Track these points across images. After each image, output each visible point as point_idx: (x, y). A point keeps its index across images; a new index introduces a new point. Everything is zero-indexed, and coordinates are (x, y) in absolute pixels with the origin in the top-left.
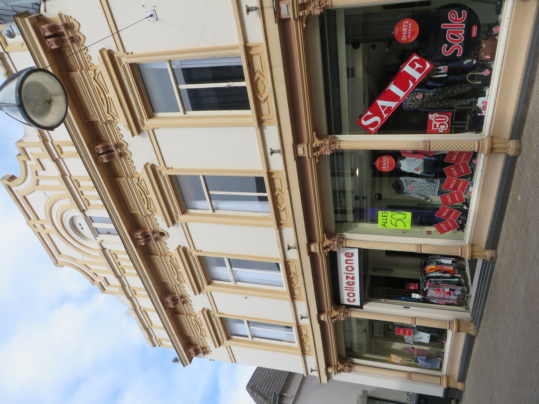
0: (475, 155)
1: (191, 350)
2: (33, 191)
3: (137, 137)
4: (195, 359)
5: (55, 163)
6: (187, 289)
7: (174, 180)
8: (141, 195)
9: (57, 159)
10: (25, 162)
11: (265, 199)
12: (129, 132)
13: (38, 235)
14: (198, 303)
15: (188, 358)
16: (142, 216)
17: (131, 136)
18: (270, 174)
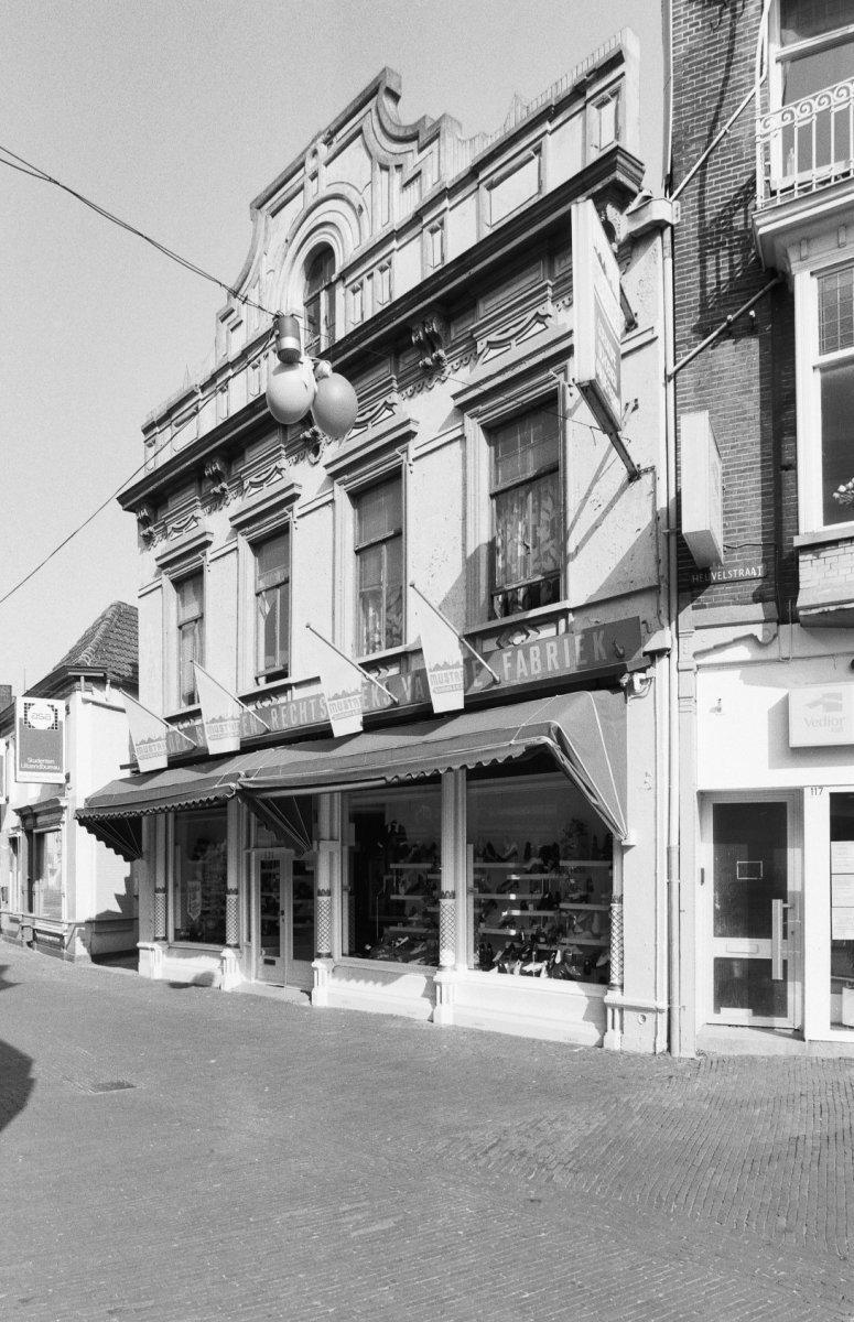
0: (593, 967)
1: (144, 513)
2: (371, 156)
3: (155, 565)
4: (132, 518)
5: (239, 354)
6: (236, 505)
7: (395, 477)
8: (370, 410)
9: (584, 94)
10: (415, 137)
11: (492, 616)
12: (460, 388)
13: (298, 164)
14: (216, 524)
15: (134, 504)
16: (166, 519)
17: (453, 393)
18: (288, 687)
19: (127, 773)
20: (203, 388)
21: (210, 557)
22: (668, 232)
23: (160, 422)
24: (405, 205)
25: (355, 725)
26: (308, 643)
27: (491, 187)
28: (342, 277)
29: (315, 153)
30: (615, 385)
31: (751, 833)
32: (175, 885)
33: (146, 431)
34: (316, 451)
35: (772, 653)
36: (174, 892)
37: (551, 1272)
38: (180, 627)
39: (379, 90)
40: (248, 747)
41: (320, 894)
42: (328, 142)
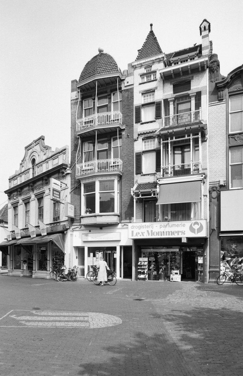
10: (45, 148)
14: (20, 199)
19: (6, 240)
20: (18, 175)
21: (19, 204)
22: (70, 174)
23: (11, 179)
24: (44, 158)
25: (46, 234)
26: (30, 221)
27: (53, 160)
28: (37, 165)
29: (33, 144)
30: (211, 233)
31: (80, 250)
32: (14, 260)
33: (9, 180)
34: (33, 191)
35: (81, 229)
36: (14, 261)
37: (6, 356)
38: (15, 215)
39: (42, 138)
40: (22, 238)
41: (34, 260)
42: (35, 143)
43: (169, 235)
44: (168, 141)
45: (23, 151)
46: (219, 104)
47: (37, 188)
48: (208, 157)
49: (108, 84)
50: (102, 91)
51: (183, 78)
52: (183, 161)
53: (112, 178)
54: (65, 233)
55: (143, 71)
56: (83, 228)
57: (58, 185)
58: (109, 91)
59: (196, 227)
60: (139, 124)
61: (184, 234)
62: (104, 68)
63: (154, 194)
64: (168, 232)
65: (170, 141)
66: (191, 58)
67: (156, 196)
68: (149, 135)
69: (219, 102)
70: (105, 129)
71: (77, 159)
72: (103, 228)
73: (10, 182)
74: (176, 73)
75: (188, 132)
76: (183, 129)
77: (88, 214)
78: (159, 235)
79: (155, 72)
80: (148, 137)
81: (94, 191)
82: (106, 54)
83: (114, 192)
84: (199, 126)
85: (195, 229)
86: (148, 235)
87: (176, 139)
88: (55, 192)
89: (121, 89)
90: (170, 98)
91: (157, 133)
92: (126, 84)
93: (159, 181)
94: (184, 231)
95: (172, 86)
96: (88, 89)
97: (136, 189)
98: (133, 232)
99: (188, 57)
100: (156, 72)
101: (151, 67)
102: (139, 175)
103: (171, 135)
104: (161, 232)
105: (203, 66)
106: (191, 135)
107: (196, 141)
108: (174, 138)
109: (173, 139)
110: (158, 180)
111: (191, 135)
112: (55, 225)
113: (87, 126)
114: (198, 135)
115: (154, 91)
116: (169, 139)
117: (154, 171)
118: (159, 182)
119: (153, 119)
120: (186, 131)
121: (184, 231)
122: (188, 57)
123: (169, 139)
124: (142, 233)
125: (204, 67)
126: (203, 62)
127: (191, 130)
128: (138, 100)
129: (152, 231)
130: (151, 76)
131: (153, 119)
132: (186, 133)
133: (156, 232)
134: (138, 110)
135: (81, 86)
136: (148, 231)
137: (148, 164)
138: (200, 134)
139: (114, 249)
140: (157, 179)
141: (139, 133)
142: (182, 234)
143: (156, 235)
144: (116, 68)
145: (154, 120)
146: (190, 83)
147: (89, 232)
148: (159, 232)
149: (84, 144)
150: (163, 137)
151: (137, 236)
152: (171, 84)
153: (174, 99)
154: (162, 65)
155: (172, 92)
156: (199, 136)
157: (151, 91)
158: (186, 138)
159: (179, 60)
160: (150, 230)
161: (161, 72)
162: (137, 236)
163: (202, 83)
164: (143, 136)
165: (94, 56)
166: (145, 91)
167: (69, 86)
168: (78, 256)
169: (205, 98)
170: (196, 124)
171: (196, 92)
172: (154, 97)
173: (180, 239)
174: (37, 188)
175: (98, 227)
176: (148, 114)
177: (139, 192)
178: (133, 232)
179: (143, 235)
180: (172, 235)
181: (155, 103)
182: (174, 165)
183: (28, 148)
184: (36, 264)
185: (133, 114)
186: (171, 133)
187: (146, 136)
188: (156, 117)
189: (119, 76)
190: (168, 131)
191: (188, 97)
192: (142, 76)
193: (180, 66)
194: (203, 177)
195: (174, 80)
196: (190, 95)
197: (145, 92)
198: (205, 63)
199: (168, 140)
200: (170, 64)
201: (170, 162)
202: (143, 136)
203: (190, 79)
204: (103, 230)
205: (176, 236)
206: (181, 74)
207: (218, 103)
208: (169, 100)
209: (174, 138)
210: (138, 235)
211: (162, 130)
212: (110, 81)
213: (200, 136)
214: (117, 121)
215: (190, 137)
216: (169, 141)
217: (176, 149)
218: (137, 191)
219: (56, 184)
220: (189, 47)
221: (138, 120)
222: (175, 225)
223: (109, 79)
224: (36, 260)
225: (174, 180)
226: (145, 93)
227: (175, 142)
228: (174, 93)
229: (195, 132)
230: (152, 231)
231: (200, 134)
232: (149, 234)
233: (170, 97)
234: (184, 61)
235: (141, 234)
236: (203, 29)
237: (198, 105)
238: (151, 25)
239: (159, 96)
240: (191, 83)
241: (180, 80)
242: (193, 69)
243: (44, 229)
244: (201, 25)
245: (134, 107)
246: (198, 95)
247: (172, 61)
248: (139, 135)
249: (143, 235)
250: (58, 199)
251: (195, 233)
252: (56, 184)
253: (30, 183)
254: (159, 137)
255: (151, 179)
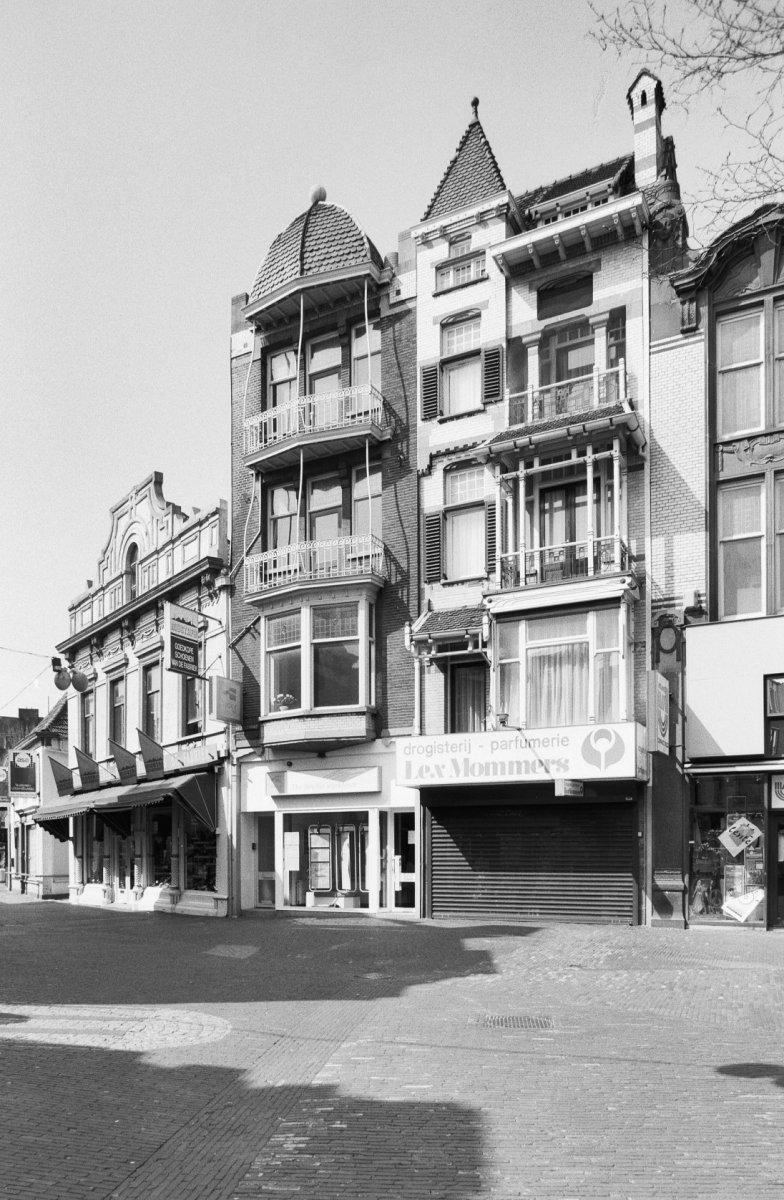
33: (70, 610)
43: (519, 772)
44: (519, 473)
45: (107, 521)
46: (686, 344)
47: (144, 633)
48: (647, 517)
49: (340, 301)
50: (320, 324)
51: (569, 267)
52: (571, 534)
53: (352, 598)
54: (216, 771)
55: (441, 251)
56: (269, 755)
57: (189, 624)
58: (342, 322)
59: (603, 746)
60: (435, 421)
61: (566, 768)
62: (323, 251)
63: (476, 646)
64: (491, 766)
65: (593, 457)
66: (596, 198)
67: (479, 650)
68: (463, 457)
69: (686, 338)
70: (312, 447)
71: (247, 545)
72: (327, 754)
73: (73, 617)
74: (547, 255)
75: (579, 442)
76: (560, 432)
77: (284, 712)
78: (487, 774)
79: (479, 254)
80: (460, 462)
81: (298, 638)
82: (332, 209)
83: (356, 642)
84: (611, 419)
85: (599, 754)
86: (454, 774)
87: (542, 463)
88: (179, 647)
89: (379, 314)
90: (529, 335)
91: (482, 448)
92: (393, 300)
93: (490, 602)
94: (567, 761)
95: (534, 296)
96: (280, 321)
97: (424, 628)
98: (409, 764)
99: (585, 199)
100: (484, 253)
101: (470, 237)
102: (437, 586)
103: (524, 455)
104: (495, 764)
105: (629, 223)
106: (589, 450)
107: (604, 467)
108: (536, 462)
109: (570, 458)
110: (488, 598)
111: (589, 450)
112: (192, 745)
113: (275, 438)
114: (612, 449)
115: (478, 316)
116: (522, 465)
117: (483, 573)
118: (489, 606)
119: (479, 405)
120: (571, 438)
121: (567, 761)
122: (555, 209)
123: (522, 465)
124: (437, 767)
125: (633, 226)
126: (627, 212)
127: (571, 438)
128: (428, 348)
129: (466, 761)
130: (469, 267)
131: (479, 405)
132: (574, 446)
133: (481, 765)
134: (432, 379)
135: (257, 314)
136: (454, 762)
137: (466, 547)
138: (616, 444)
139: (360, 819)
140: (485, 596)
141: (434, 452)
142: (558, 770)
143: (481, 773)
144: (359, 248)
145: (480, 406)
146: (590, 284)
147: (286, 767)
148: (487, 764)
149: (273, 492)
150: (503, 460)
151: (422, 777)
152: (531, 289)
153: (539, 336)
154: (499, 228)
155: (534, 313)
156: (613, 452)
157: (470, 314)
158: (575, 460)
159: (588, 198)
160: (460, 757)
161: (496, 251)
162: (534, 772)
163: (622, 283)
164: (446, 462)
165: (298, 216)
166: (451, 317)
167: (225, 314)
168: (257, 842)
169: (636, 329)
170: (606, 412)
171: (609, 308)
172: (477, 335)
173: (550, 786)
174: (144, 633)
175: (312, 751)
176: (465, 388)
177: (467, 633)
178: (409, 764)
179: (441, 775)
180: (527, 772)
181: (483, 354)
182: (572, 544)
183: (117, 511)
184: (182, 870)
185: (416, 392)
186: (523, 448)
187: (454, 459)
188: (487, 397)
189: (368, 275)
190: (515, 443)
191: (584, 326)
192: (441, 268)
193: (564, 225)
194: (625, 586)
195: (541, 276)
196: (591, 321)
197: (451, 320)
198: (634, 215)
199: (516, 469)
200: (530, 223)
201: (521, 541)
202: (446, 462)
203: (589, 268)
204: (329, 760)
205: (539, 776)
206: (562, 255)
207: (681, 339)
208: (524, 340)
209: (536, 462)
210: (425, 775)
211: (500, 438)
212: (345, 292)
213: (616, 452)
214: (362, 418)
215: (586, 458)
216: (522, 472)
217: (547, 495)
218: (424, 636)
219: (183, 621)
220: (615, 158)
221: (432, 411)
222: (538, 739)
223: (339, 285)
224: (144, 854)
225: (533, 597)
226: (449, 324)
227: (545, 475)
228: (541, 317)
229: (601, 440)
230: (466, 761)
231: (616, 444)
232: (458, 771)
233: (530, 332)
234: (576, 211)
235: (433, 770)
236: (637, 101)
237: (619, 349)
238: (475, 103)
239: (489, 334)
240: (594, 281)
241: (556, 277)
242: (597, 238)
243: (154, 760)
244: (631, 90)
245: (418, 369)
246: (617, 320)
247: (536, 213)
248: (432, 457)
249: (441, 775)
250: (192, 668)
251: (599, 766)
252: (183, 621)
253: (123, 619)
254: (493, 459)
255: (469, 597)
